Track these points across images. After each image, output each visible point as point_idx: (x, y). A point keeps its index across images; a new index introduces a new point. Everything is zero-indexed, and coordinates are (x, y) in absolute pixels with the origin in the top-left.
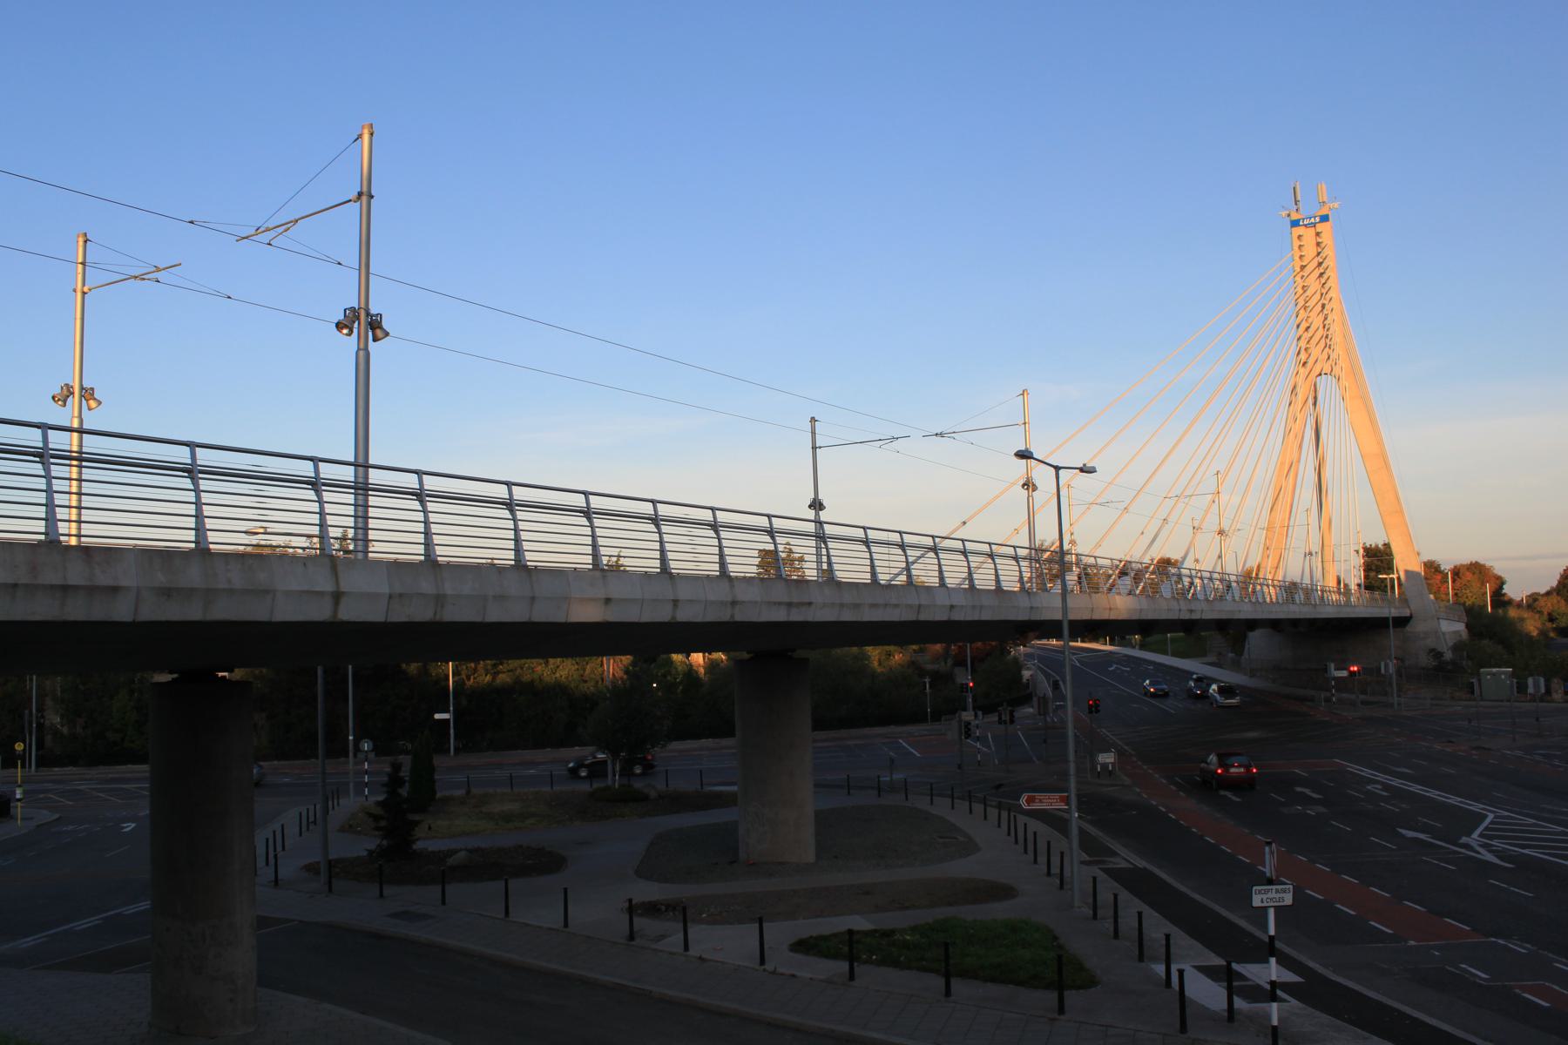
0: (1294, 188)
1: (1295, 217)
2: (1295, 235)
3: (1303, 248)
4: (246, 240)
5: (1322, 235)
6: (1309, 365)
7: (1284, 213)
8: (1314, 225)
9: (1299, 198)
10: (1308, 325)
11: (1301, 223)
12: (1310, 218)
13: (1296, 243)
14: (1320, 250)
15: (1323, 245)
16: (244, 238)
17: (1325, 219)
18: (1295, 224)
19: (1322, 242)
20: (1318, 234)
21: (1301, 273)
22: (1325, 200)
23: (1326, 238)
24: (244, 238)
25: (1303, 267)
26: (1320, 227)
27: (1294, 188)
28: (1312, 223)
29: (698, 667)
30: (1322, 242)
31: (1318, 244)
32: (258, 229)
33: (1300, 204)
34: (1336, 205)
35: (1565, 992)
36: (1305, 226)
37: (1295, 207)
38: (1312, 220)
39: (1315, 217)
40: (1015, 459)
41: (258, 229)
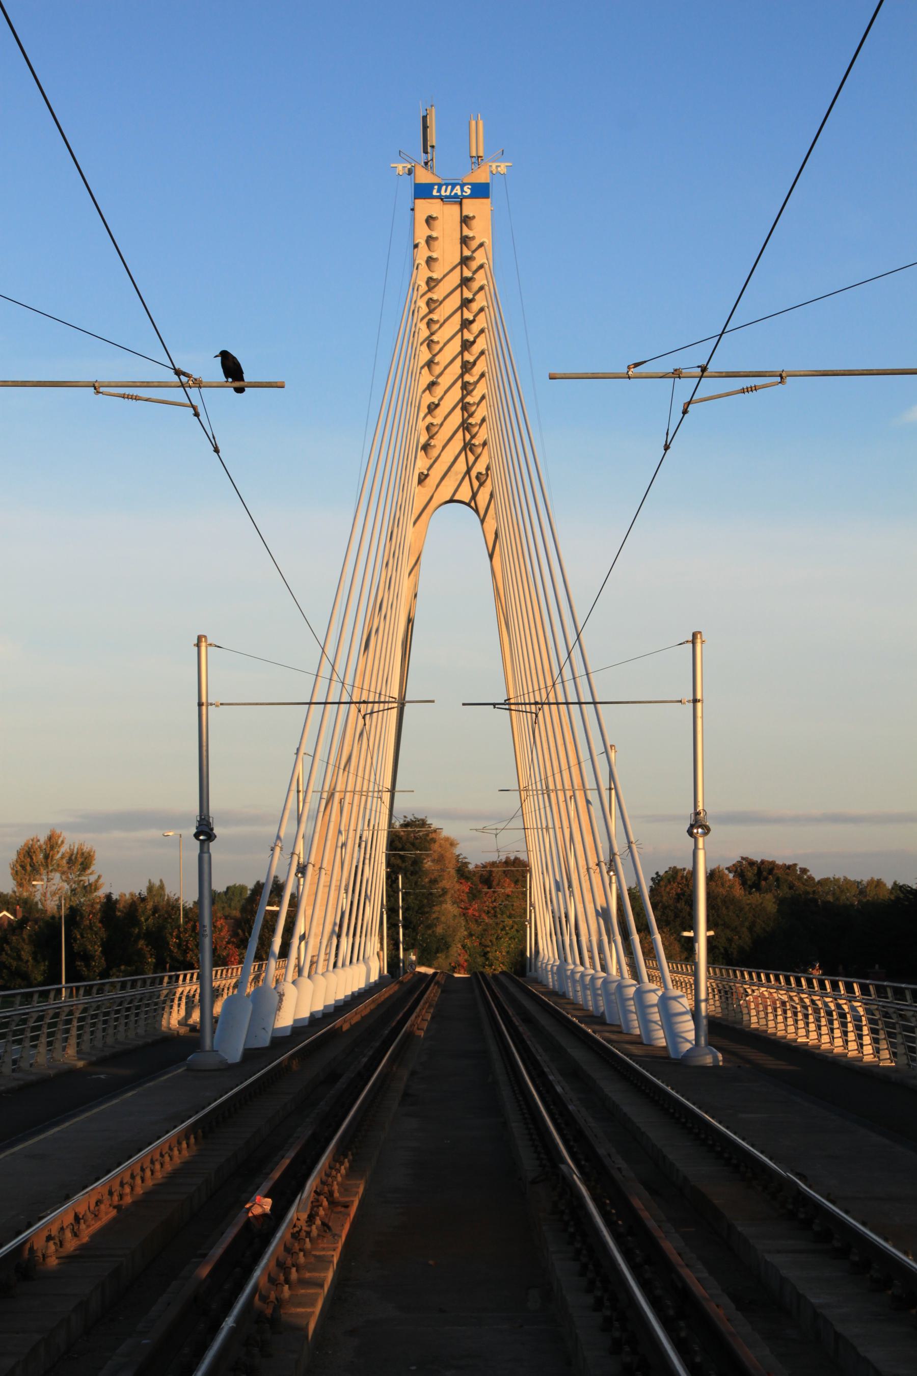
0: (425, 118)
1: (423, 176)
2: (421, 217)
3: (436, 244)
4: (582, 636)
5: (474, 223)
6: (434, 453)
7: (401, 167)
8: (459, 201)
9: (433, 139)
10: (432, 379)
11: (435, 193)
12: (454, 186)
13: (422, 232)
14: (467, 253)
15: (474, 244)
16: (578, 636)
17: (481, 191)
18: (423, 191)
19: (473, 238)
20: (465, 220)
21: (429, 295)
22: (481, 154)
23: (480, 231)
24: (578, 636)
25: (432, 283)
26: (471, 207)
27: (425, 118)
28: (456, 196)
29: (76, 906)
30: (473, 238)
31: (465, 240)
32: (636, 365)
33: (436, 155)
34: (503, 169)
35: (908, 1260)
36: (441, 198)
37: (423, 157)
38: (458, 190)
39: (462, 186)
40: (894, 881)
41: (636, 365)
